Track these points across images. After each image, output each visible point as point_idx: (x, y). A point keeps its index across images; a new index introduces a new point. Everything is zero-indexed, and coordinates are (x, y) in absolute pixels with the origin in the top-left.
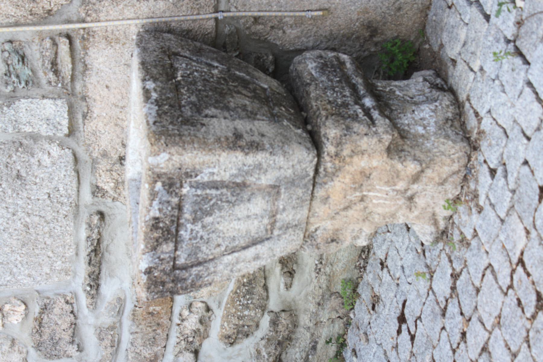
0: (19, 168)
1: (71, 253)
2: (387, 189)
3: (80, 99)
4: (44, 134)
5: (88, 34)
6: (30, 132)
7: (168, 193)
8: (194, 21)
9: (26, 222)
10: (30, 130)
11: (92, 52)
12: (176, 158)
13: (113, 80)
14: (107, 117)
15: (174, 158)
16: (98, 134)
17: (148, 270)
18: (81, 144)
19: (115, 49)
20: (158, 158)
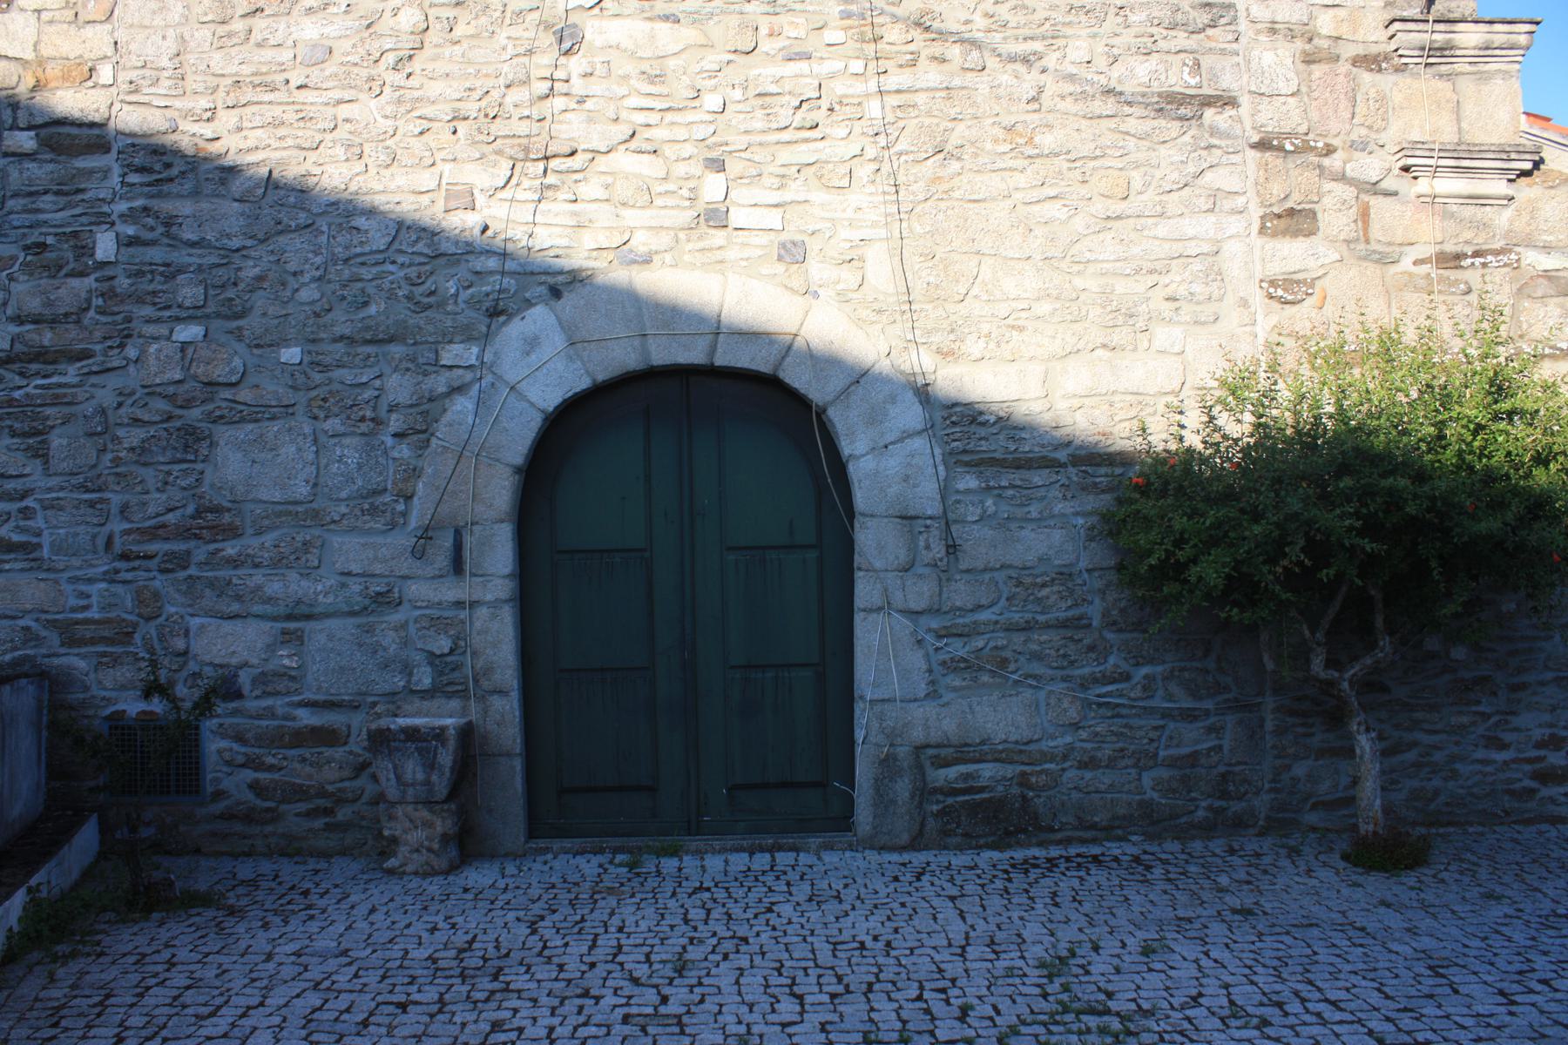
1: (332, 691)
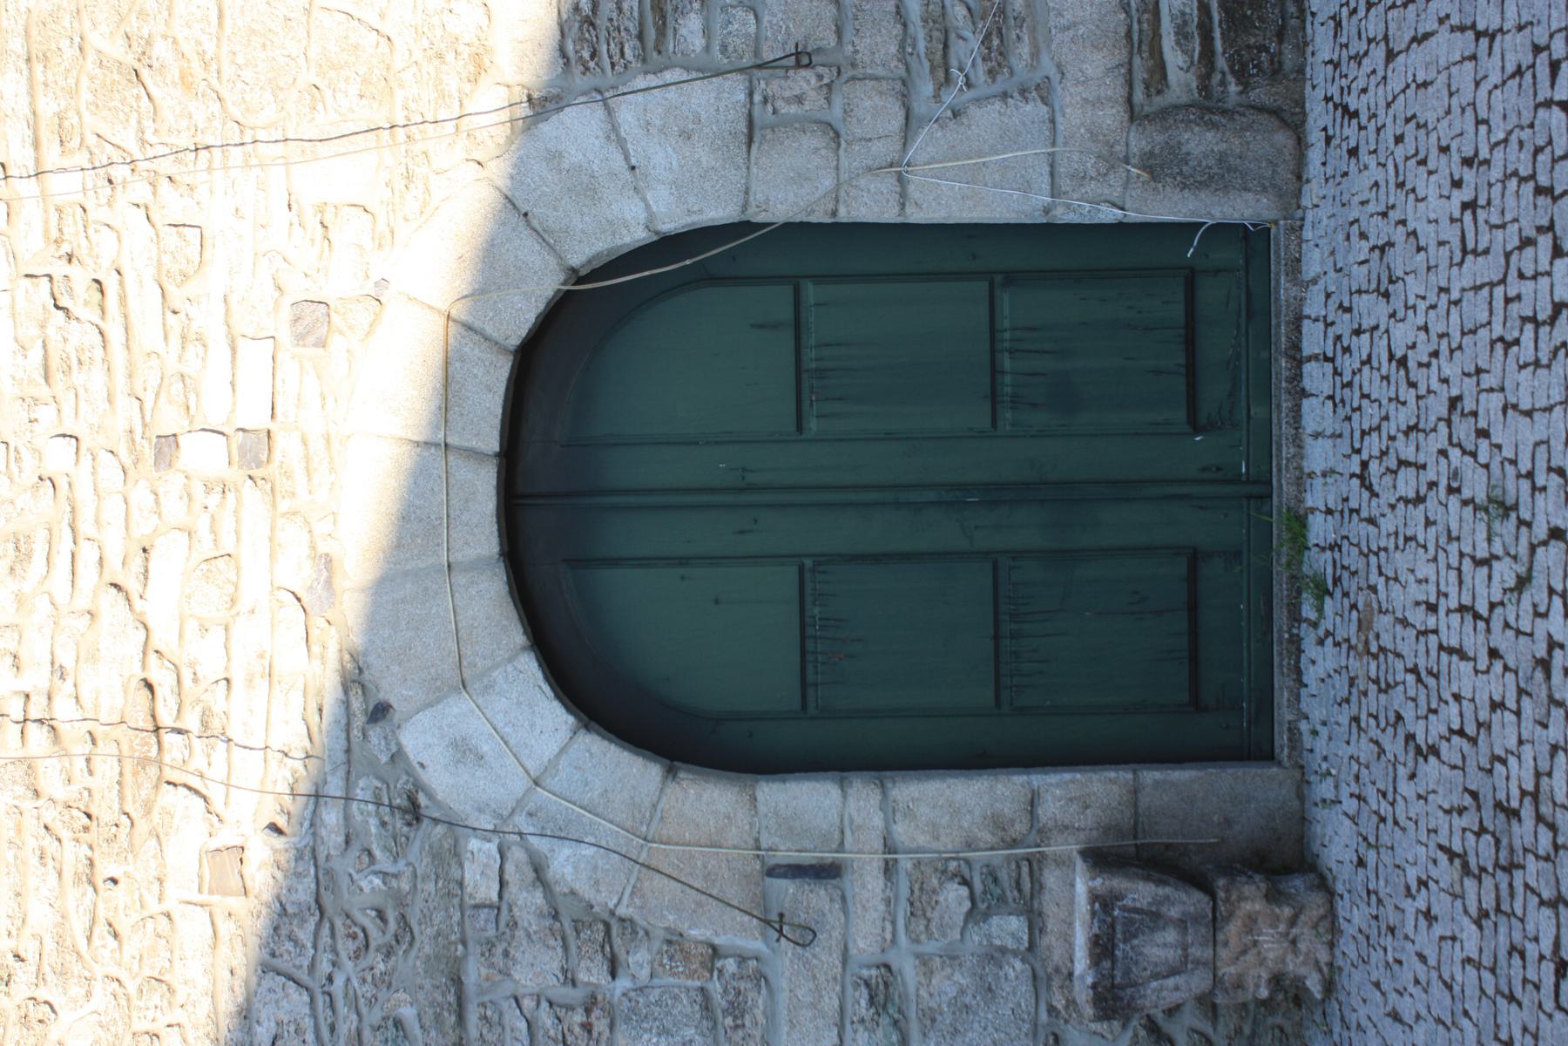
4: (1010, 947)
8: (1119, 846)
11: (1046, 873)
12: (1107, 883)
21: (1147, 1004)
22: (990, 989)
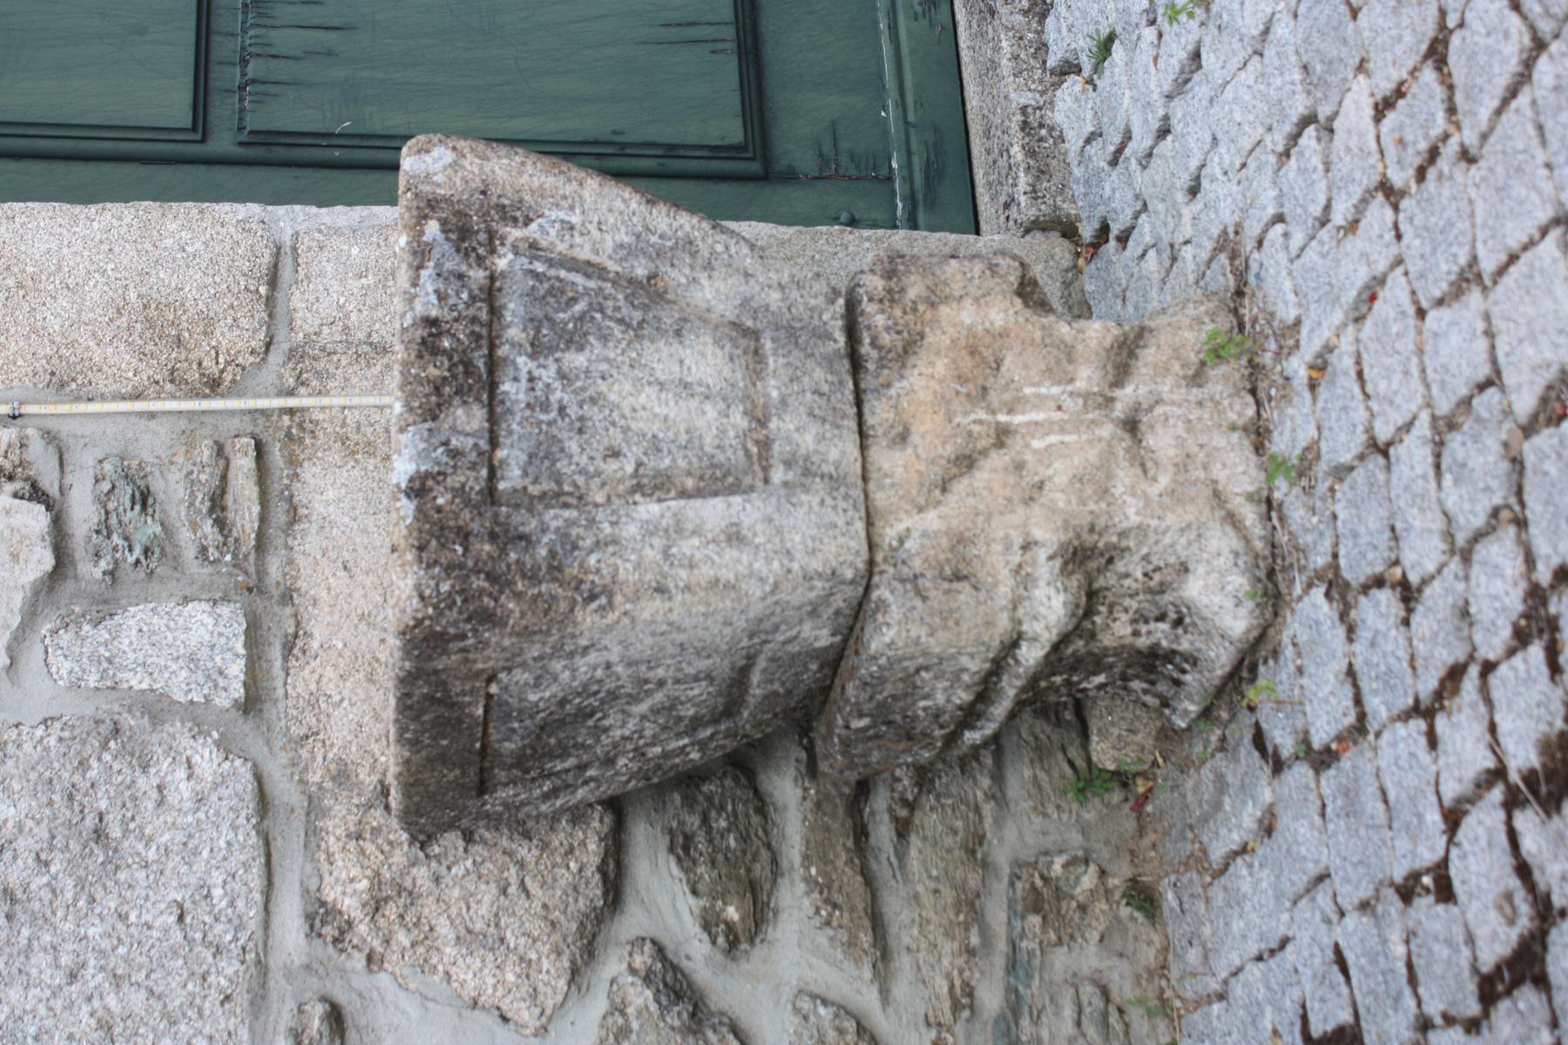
0: (103, 805)
2: (1055, 390)
3: (279, 603)
4: (179, 697)
5: (301, 426)
6: (143, 691)
7: (458, 251)
9: (107, 1010)
10: (144, 686)
11: (308, 472)
13: (361, 550)
14: (347, 653)
15: (466, 163)
16: (323, 706)
17: (417, 485)
18: (279, 742)
19: (365, 469)
20: (428, 158)
21: (626, 572)
22: (99, 835)
